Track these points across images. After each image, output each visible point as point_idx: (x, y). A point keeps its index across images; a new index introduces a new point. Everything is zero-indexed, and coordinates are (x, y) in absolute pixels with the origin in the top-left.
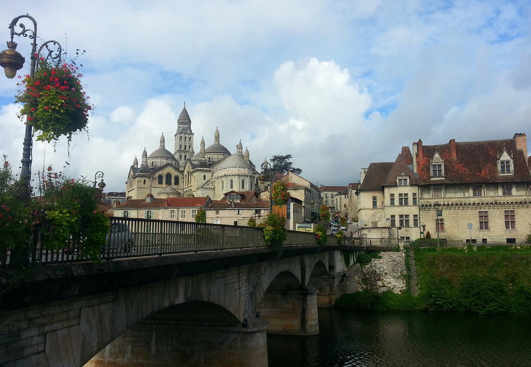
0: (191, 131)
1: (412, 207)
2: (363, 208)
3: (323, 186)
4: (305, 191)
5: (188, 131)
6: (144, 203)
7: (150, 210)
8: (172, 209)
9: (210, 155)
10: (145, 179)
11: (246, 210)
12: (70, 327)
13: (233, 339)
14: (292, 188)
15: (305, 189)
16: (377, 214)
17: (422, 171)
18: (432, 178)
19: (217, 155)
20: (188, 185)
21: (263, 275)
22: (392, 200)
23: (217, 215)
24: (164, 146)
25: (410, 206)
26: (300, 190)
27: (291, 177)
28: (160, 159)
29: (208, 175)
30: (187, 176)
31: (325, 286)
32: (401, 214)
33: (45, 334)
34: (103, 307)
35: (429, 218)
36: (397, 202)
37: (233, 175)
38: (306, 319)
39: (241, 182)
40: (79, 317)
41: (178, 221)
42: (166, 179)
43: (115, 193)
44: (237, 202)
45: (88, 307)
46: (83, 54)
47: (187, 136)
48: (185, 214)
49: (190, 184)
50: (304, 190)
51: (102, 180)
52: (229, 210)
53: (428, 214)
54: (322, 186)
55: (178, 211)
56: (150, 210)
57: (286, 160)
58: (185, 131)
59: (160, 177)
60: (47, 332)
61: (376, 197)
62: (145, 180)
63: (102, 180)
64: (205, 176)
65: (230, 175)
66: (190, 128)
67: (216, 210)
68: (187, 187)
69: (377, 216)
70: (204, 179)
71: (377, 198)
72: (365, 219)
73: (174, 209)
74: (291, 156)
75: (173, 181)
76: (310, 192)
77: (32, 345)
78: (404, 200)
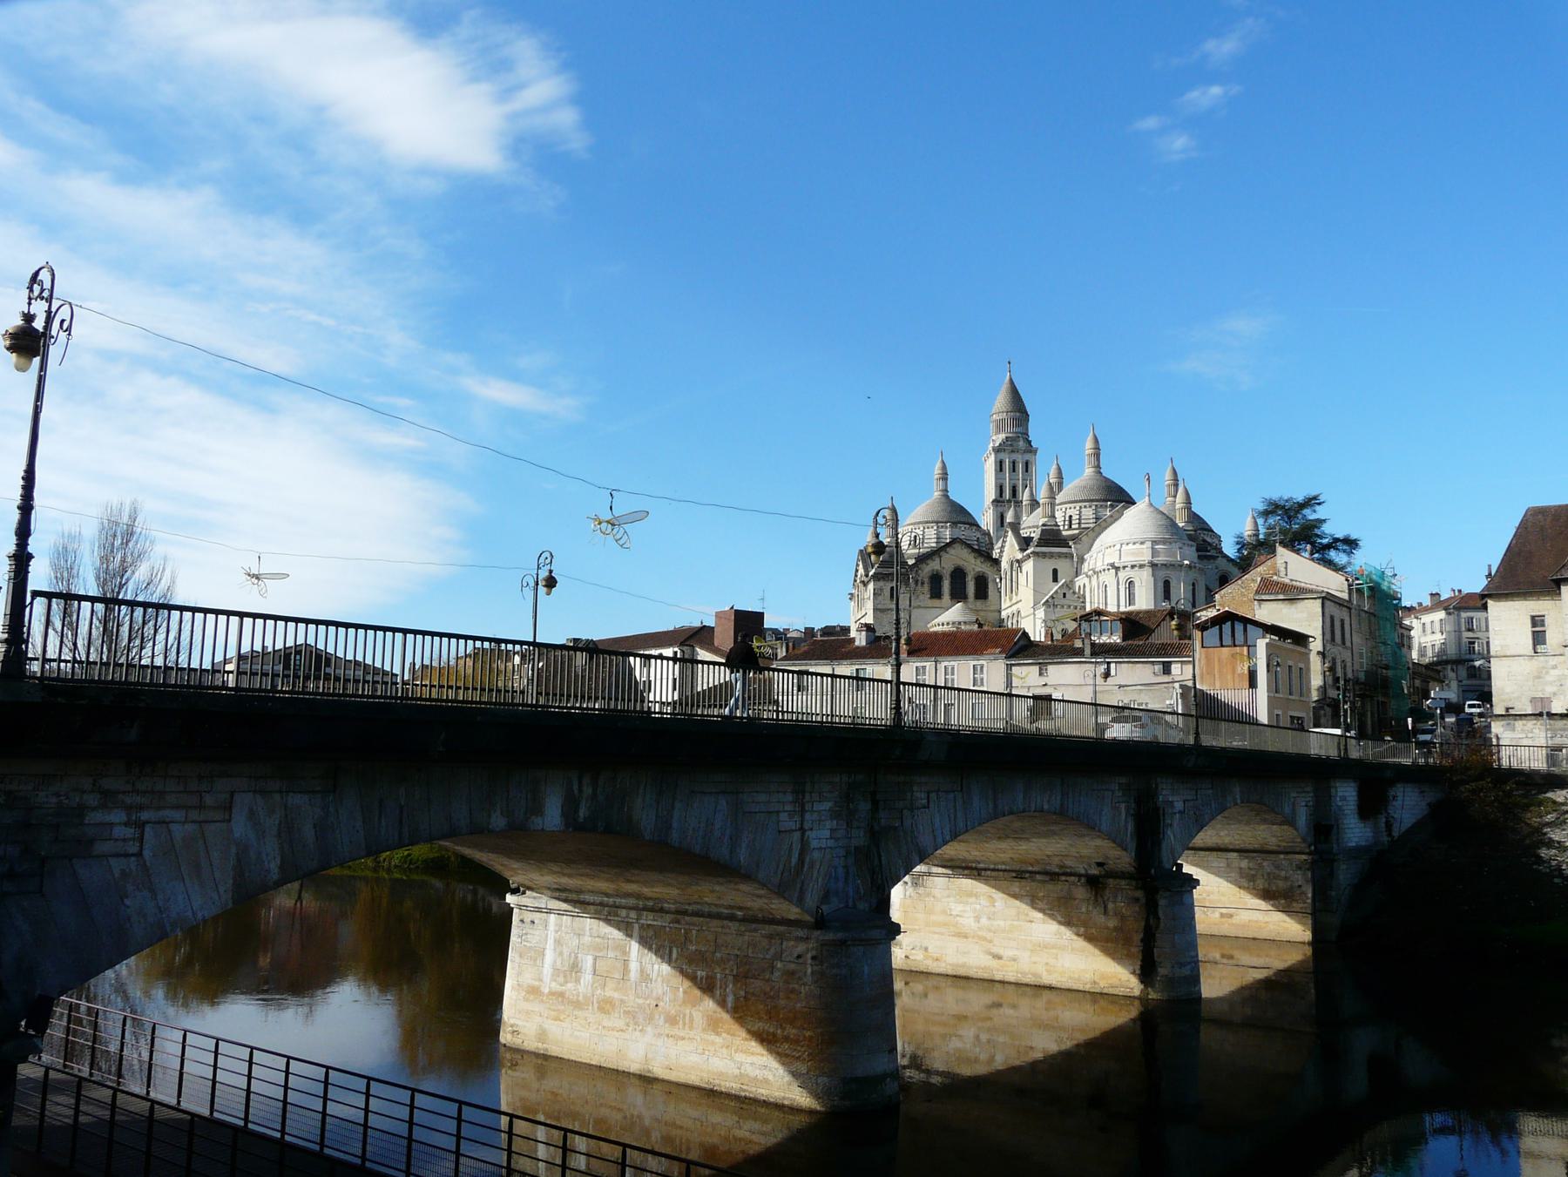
0: (1030, 442)
2: (1498, 654)
3: (1460, 591)
6: (849, 648)
7: (863, 667)
8: (919, 664)
9: (1072, 510)
11: (1126, 665)
12: (206, 822)
13: (796, 955)
14: (1281, 597)
15: (1323, 598)
16: (1547, 673)
19: (1094, 507)
20: (1011, 599)
21: (918, 808)
23: (1042, 681)
24: (947, 491)
26: (1306, 601)
27: (1286, 563)
28: (935, 528)
29: (1064, 567)
30: (1009, 574)
31: (1300, 883)
33: (141, 825)
34: (296, 800)
37: (1135, 566)
38: (1156, 959)
39: (1161, 585)
40: (228, 807)
41: (537, 641)
42: (952, 583)
43: (838, 629)
44: (1101, 641)
45: (255, 792)
48: (955, 677)
49: (1017, 595)
50: (1321, 600)
51: (551, 571)
52: (1078, 665)
54: (1457, 594)
55: (936, 670)
56: (863, 667)
57: (1307, 512)
58: (1011, 445)
59: (936, 579)
60: (148, 822)
61: (1544, 616)
63: (551, 571)
64: (1055, 572)
65: (1126, 564)
67: (1040, 663)
68: (1008, 604)
69: (1548, 678)
70: (1055, 580)
71: (1548, 621)
72: (1508, 690)
73: (925, 664)
74: (1322, 498)
75: (971, 588)
76: (1350, 609)
77: (110, 839)
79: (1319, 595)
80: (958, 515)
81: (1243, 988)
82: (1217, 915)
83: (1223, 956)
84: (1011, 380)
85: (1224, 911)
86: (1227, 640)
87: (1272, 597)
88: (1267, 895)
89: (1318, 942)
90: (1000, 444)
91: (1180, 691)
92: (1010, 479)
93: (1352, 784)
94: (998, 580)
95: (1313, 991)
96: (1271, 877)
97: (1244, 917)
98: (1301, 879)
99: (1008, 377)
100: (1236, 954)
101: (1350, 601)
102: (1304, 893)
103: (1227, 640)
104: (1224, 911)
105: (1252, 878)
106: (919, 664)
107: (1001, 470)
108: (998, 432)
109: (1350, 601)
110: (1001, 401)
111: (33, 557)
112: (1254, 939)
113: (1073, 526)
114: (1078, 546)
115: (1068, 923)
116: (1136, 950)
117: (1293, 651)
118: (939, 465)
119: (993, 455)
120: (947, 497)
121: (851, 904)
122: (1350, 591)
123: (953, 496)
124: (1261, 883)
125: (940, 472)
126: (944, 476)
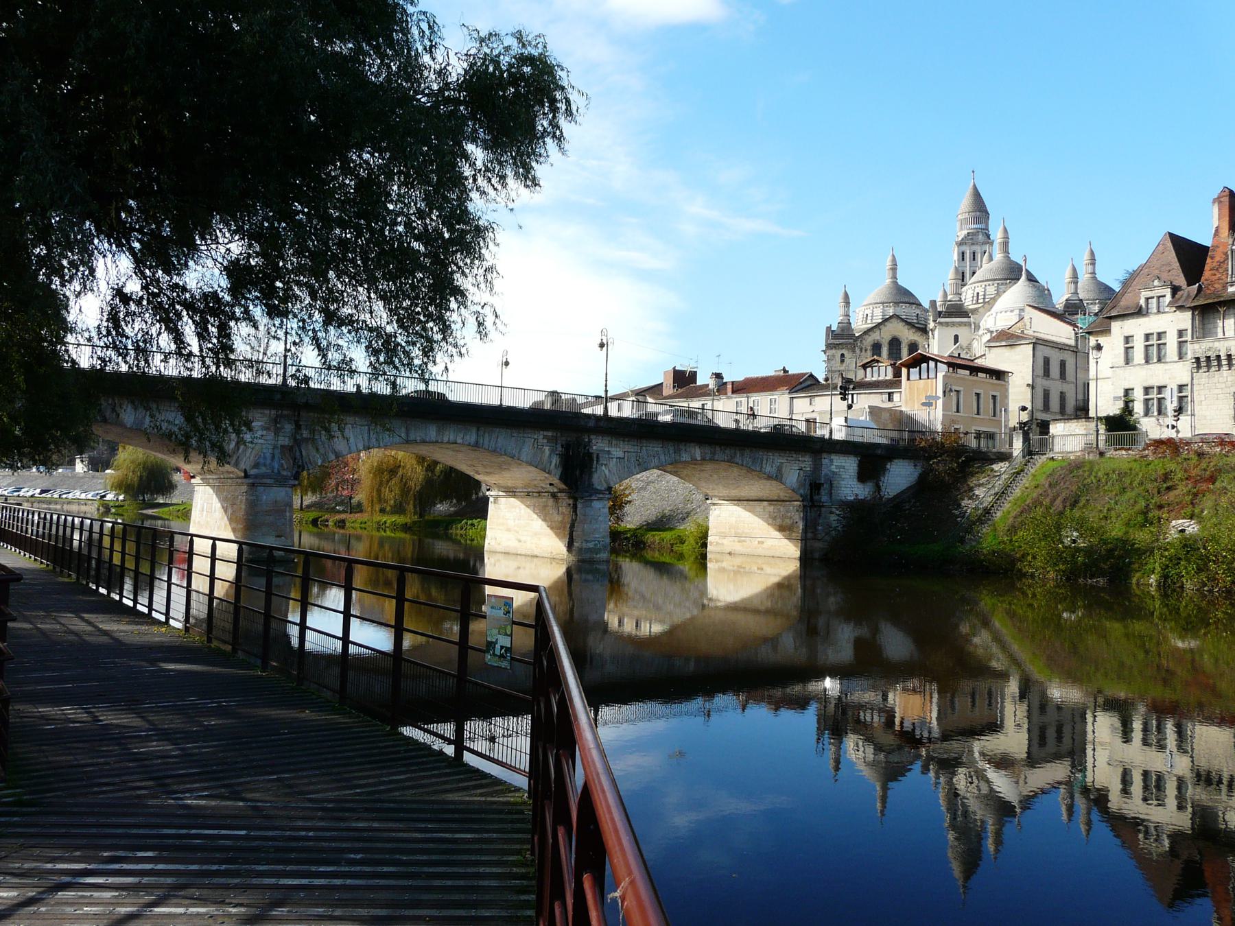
0: (988, 236)
1: (1175, 365)
4: (1034, 348)
5: (980, 236)
8: (738, 399)
10: (844, 351)
14: (1004, 344)
17: (1217, 270)
18: (1232, 286)
19: (996, 285)
22: (1128, 350)
25: (1170, 362)
29: (963, 333)
32: (1146, 385)
35: (1216, 391)
36: (1138, 354)
46: (552, 165)
47: (978, 249)
48: (777, 406)
50: (1031, 345)
53: (1215, 380)
58: (972, 239)
59: (876, 348)
62: (842, 355)
66: (987, 230)
78: (1155, 349)
79: (1031, 341)
80: (902, 296)
81: (767, 588)
82: (757, 542)
83: (758, 569)
84: (975, 188)
85: (760, 539)
86: (924, 375)
87: (998, 344)
88: (781, 529)
89: (805, 559)
90: (963, 239)
91: (868, 410)
92: (970, 267)
93: (853, 459)
94: (926, 346)
95: (800, 590)
96: (784, 517)
97: (769, 543)
98: (798, 518)
99: (972, 184)
100: (764, 567)
101: (1076, 346)
102: (798, 527)
103: (924, 375)
104: (760, 539)
105: (774, 518)
106: (738, 399)
107: (963, 259)
108: (961, 229)
109: (1076, 346)
110: (965, 203)
111: (695, 373)
112: (773, 557)
113: (980, 301)
114: (975, 316)
115: (544, 520)
116: (567, 532)
117: (996, 384)
118: (890, 258)
119: (956, 248)
120: (1095, 278)
121: (276, 471)
122: (1077, 338)
123: (900, 282)
124: (779, 521)
125: (891, 263)
126: (894, 268)
